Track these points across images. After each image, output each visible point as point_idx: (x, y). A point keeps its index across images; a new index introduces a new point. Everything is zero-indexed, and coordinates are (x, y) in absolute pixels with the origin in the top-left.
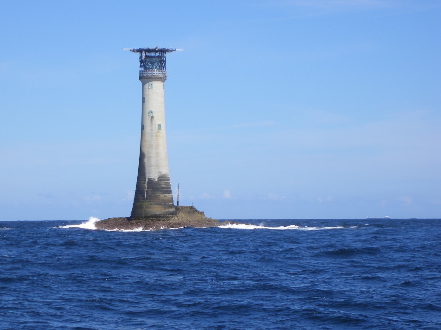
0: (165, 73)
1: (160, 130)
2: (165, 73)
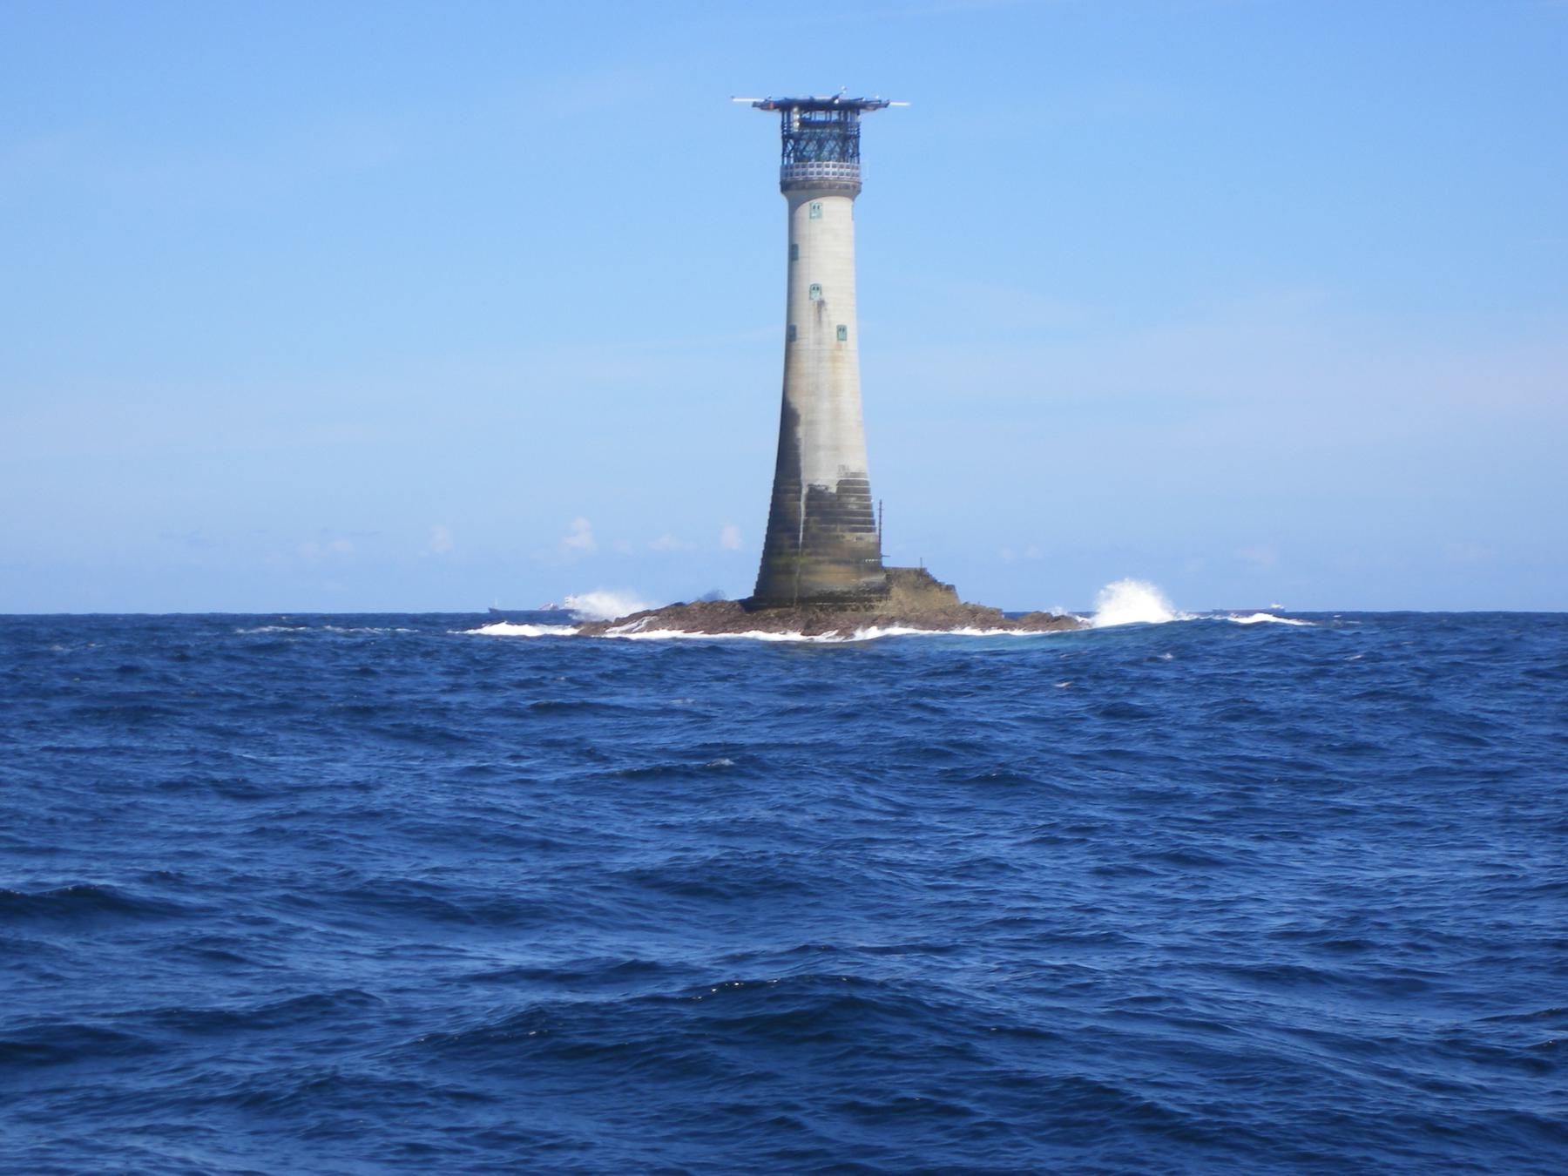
1: (843, 343)
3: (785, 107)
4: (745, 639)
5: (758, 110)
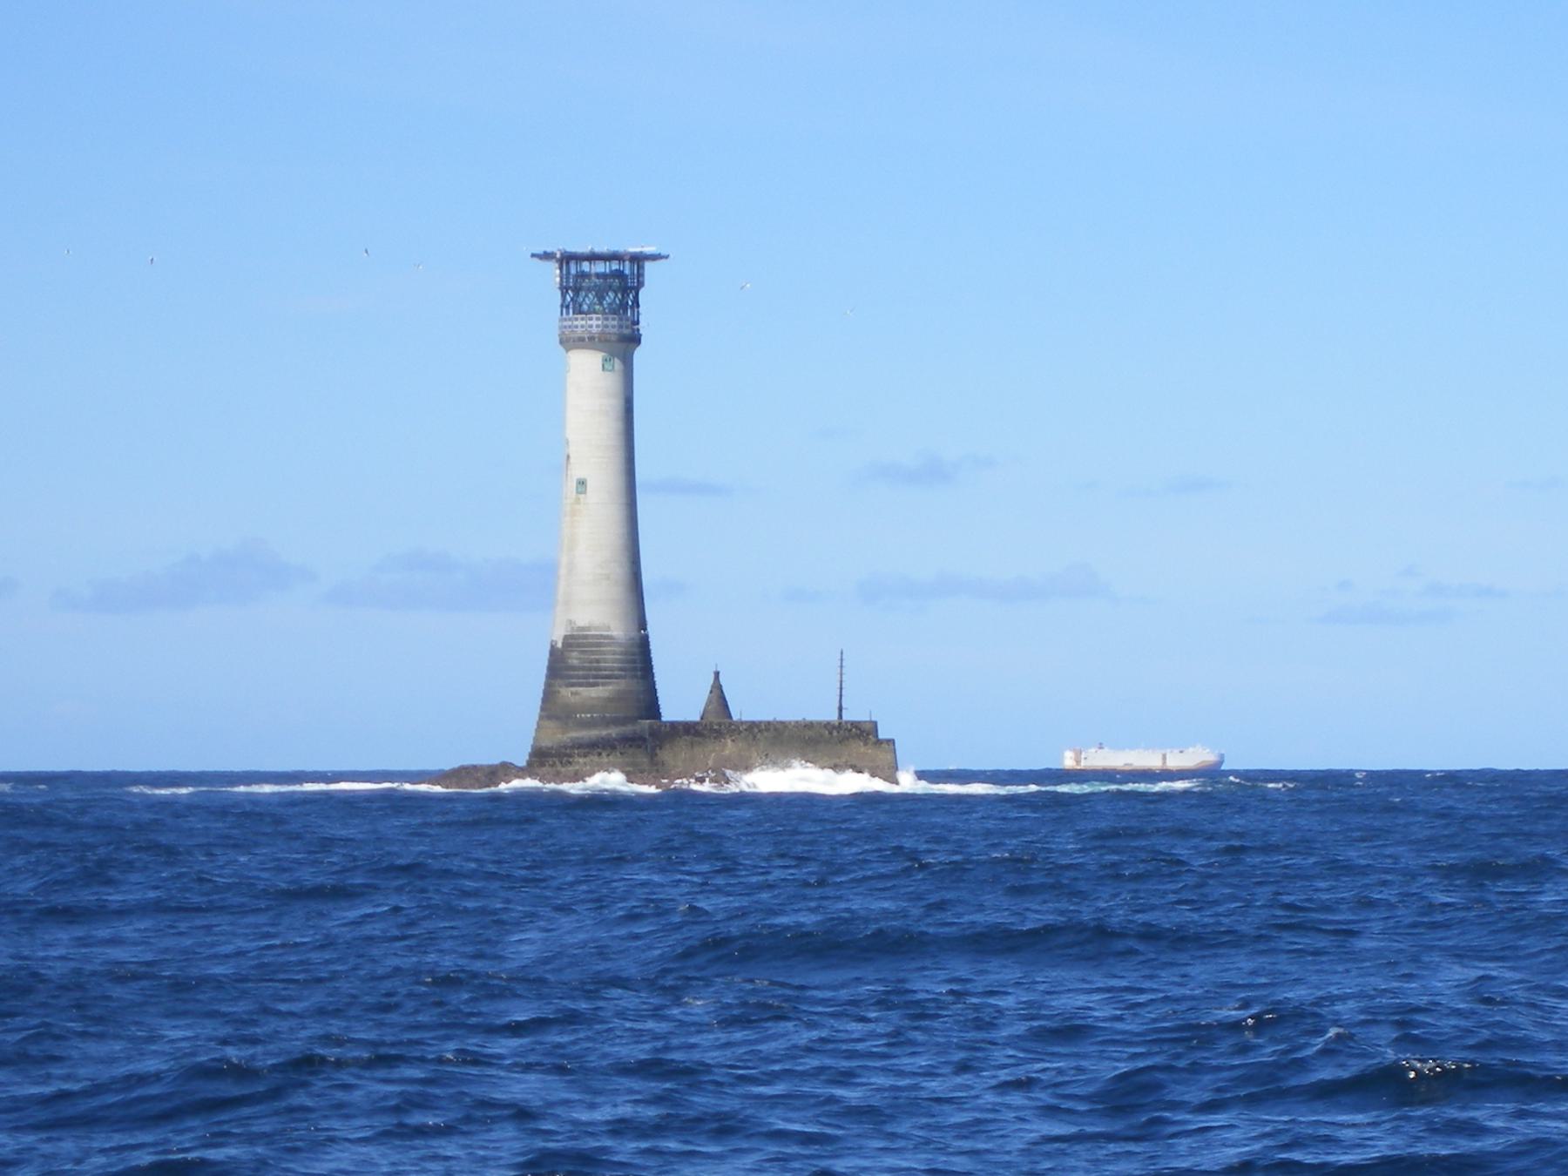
0: (565, 323)
1: (582, 496)
2: (565, 323)
3: (567, 259)
4: (154, 795)
5: (536, 260)
